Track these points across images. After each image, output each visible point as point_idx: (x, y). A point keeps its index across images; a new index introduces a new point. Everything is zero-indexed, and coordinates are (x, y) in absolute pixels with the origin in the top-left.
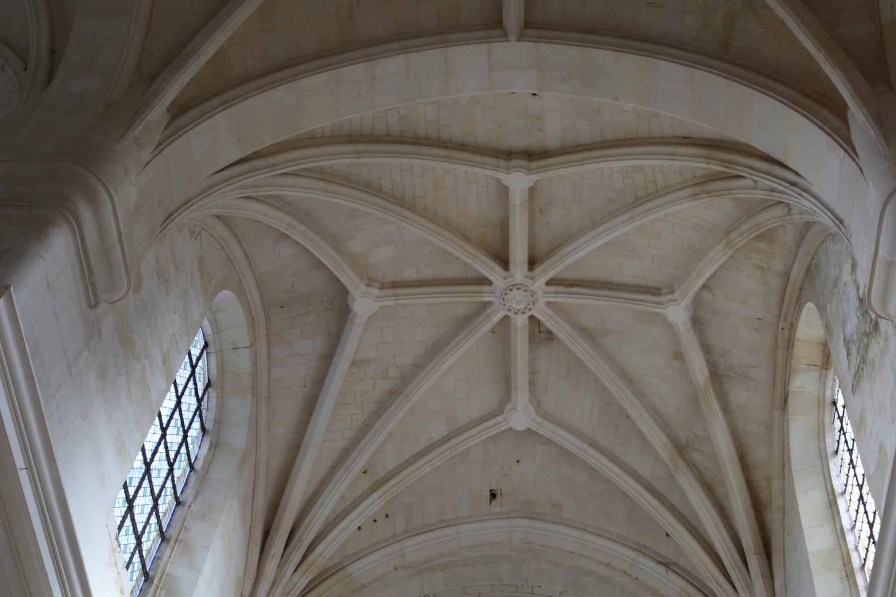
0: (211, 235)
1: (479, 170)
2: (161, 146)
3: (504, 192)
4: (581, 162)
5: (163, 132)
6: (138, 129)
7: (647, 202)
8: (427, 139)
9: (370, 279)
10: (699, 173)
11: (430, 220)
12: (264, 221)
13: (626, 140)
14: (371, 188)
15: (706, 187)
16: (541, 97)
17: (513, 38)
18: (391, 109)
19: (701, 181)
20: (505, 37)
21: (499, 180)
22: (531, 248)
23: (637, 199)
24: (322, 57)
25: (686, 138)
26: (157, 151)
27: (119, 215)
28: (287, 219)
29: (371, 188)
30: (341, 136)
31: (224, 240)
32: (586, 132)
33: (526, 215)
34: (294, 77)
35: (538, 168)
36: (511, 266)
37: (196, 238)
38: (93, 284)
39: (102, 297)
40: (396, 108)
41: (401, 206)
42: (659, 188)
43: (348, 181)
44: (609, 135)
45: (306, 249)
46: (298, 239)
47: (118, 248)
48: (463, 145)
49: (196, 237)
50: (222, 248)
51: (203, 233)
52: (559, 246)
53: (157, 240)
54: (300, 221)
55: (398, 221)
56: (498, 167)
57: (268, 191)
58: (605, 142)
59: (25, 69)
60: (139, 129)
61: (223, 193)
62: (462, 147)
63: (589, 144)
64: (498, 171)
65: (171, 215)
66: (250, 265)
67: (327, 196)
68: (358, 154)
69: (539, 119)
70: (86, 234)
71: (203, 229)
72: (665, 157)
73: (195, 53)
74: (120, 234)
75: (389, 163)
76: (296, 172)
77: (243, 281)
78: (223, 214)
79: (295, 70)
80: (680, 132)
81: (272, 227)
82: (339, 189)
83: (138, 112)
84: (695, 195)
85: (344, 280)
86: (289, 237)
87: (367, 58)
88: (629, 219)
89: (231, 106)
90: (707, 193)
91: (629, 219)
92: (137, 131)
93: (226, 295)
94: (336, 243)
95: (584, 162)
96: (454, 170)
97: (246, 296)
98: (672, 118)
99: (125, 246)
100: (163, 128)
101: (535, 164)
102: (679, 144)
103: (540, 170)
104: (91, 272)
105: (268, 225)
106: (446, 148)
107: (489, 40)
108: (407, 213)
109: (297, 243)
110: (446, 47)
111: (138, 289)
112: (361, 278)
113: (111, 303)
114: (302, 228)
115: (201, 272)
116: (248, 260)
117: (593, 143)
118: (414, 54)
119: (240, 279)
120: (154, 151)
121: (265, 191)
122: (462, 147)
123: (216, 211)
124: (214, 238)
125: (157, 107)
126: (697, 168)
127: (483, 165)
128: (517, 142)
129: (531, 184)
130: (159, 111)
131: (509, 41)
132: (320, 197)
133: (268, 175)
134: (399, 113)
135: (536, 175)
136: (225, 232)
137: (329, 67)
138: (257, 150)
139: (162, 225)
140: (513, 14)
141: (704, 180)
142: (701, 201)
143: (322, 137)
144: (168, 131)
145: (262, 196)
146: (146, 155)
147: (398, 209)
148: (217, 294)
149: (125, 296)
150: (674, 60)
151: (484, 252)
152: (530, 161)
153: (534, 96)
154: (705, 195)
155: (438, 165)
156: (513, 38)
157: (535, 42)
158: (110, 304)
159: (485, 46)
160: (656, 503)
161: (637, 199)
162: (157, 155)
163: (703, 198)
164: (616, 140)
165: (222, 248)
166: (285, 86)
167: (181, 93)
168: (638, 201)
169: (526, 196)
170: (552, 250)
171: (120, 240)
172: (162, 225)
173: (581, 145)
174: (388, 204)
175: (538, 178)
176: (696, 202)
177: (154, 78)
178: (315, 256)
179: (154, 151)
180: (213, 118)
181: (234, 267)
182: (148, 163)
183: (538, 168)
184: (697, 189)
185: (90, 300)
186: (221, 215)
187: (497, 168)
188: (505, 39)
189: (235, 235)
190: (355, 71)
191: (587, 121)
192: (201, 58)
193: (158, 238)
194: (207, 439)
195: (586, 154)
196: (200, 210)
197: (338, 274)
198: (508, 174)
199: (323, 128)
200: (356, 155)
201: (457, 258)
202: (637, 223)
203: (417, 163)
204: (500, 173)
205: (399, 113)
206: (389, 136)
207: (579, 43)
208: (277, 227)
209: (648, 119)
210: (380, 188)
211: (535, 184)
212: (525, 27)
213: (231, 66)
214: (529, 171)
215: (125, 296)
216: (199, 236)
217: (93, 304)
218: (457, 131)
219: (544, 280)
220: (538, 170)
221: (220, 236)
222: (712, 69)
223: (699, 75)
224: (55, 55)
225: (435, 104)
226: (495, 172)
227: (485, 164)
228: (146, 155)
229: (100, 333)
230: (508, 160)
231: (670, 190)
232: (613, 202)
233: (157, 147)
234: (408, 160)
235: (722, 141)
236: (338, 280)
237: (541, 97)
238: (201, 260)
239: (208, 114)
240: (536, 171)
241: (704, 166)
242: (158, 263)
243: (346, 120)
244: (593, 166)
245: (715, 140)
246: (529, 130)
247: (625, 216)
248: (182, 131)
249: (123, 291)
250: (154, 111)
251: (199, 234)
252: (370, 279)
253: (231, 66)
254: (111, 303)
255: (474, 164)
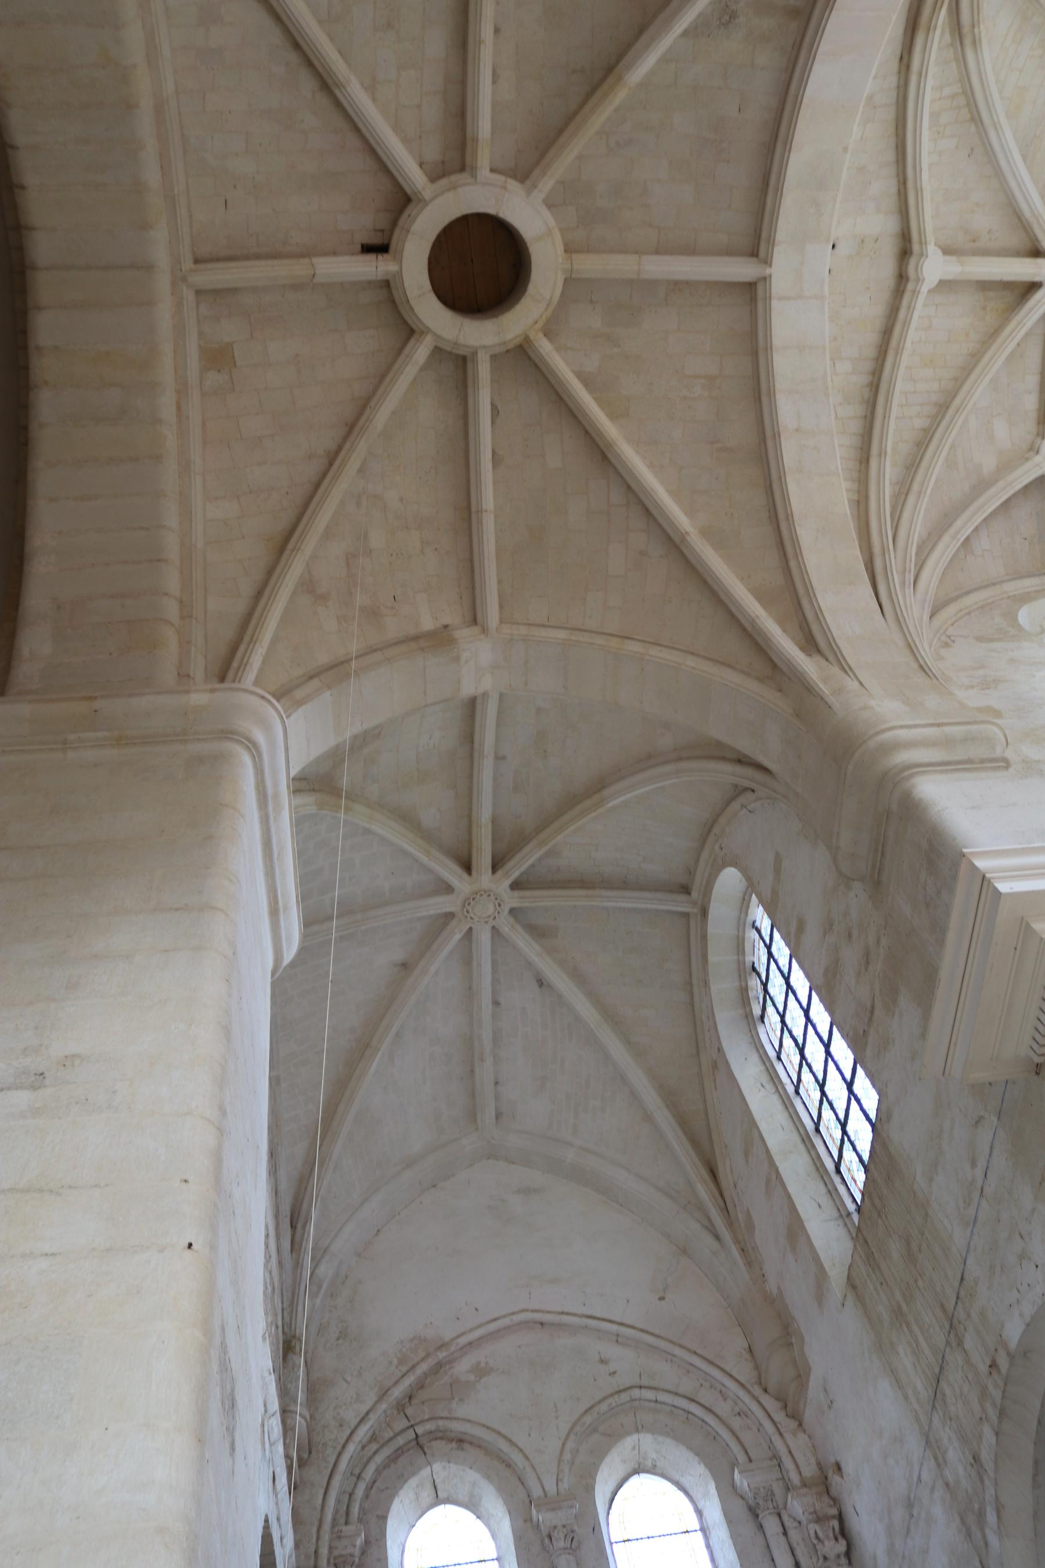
0: (952, 625)
1: (916, 314)
2: (846, 669)
3: (945, 286)
4: (919, 191)
5: (832, 664)
6: (824, 689)
7: (976, 106)
8: (874, 373)
9: (1030, 449)
10: (947, 38)
11: (968, 375)
12: (946, 564)
13: (897, 135)
14: (923, 442)
15: (966, 29)
16: (837, 239)
17: (768, 271)
18: (836, 413)
19: (957, 36)
20: (765, 279)
21: (929, 291)
22: (1019, 254)
23: (973, 119)
24: (771, 485)
25: (901, 58)
26: (850, 673)
27: (911, 723)
28: (946, 538)
29: (923, 442)
30: (860, 471)
31: (961, 610)
32: (884, 184)
33: (977, 259)
34: (789, 517)
35: (921, 243)
36: (1037, 279)
37: (954, 642)
38: (982, 761)
39: (998, 752)
40: (834, 407)
41: (947, 408)
42: (961, 90)
43: (912, 466)
44: (890, 156)
45: (985, 520)
46: (971, 529)
47: (947, 729)
48: (885, 333)
49: (952, 640)
50: (969, 613)
51: (948, 633)
52: (1019, 218)
53: (946, 686)
54: (950, 525)
55: (965, 412)
56: (914, 291)
57: (911, 556)
58: (897, 161)
59: (753, 791)
60: (824, 688)
61: (906, 606)
62: (887, 332)
63: (899, 181)
64: (919, 292)
65: (921, 667)
66: (994, 584)
67: (925, 493)
68: (882, 453)
69: (863, 241)
70: (927, 760)
71: (945, 632)
72: (922, 86)
73: (753, 620)
74: (931, 725)
75: (897, 418)
76: (895, 525)
77: (1012, 594)
78: (930, 609)
79: (781, 516)
80: (894, 65)
81: (954, 555)
82: (919, 478)
83: (808, 688)
84: (975, 43)
85: (1026, 481)
86: (968, 539)
87: (776, 436)
88: (996, 129)
89: (812, 588)
90: (973, 27)
91: (996, 129)
92: (827, 692)
93: (1024, 616)
94: (981, 486)
95: (919, 188)
96: (912, 343)
97: (1028, 593)
98: (875, 77)
99: (946, 721)
100: (827, 663)
101: (916, 247)
102: (908, 67)
103: (923, 241)
104: (969, 761)
105: (951, 561)
106: (886, 351)
107: (768, 298)
108: (957, 401)
109: (976, 529)
110: (771, 347)
111: (998, 714)
112: (1027, 459)
113: (1007, 744)
114: (959, 523)
115: (992, 640)
116: (988, 586)
117: (898, 176)
118: (777, 384)
119: (1009, 597)
120: (849, 676)
121: (911, 561)
122: (887, 332)
123: (926, 617)
124: (956, 621)
125: (805, 667)
126: (940, 42)
127: (911, 308)
128: (887, 269)
129: (940, 252)
130: (808, 666)
131: (770, 276)
132: (926, 500)
133: (892, 556)
134: (840, 404)
135: (928, 246)
136: (951, 610)
137: (783, 479)
138: (863, 566)
139: (930, 678)
140: (742, 270)
141: (957, 32)
142: (983, 35)
143: (859, 492)
144: (831, 658)
145: (916, 564)
146: (852, 684)
147: (951, 412)
148: (1020, 625)
149: (1002, 729)
150: (805, 78)
151: (1014, 313)
152: (911, 253)
153: (836, 247)
154: (976, 30)
155: (905, 360)
156: (768, 271)
157: (773, 245)
158: (1009, 746)
159: (775, 303)
160: (932, 52)
161: (973, 119)
162: (854, 674)
163: (980, 33)
164: (897, 147)
165: (969, 613)
166: (797, 528)
167: (793, 639)
168: (976, 118)
169: (954, 258)
170: (1024, 228)
171: (939, 725)
172: (930, 678)
173: (899, 190)
174: (944, 423)
175: (933, 243)
176: (984, 42)
177: (775, 666)
178: (994, 510)
179: (849, 676)
180: (823, 609)
181: (993, 602)
182: (861, 683)
183: (921, 243)
184: (968, 41)
185: (999, 767)
186: (931, 612)
187: (915, 293)
188: (768, 279)
189: (954, 599)
190: (790, 451)
191: (870, 183)
192: (759, 615)
193: (945, 684)
194: (749, 965)
195: (910, 184)
196: (921, 637)
197: (1019, 486)
198: (924, 280)
199: (848, 490)
200: (883, 456)
201: (1018, 345)
202: (1003, 119)
203: (900, 386)
204: (922, 290)
205: (840, 404)
206: (866, 416)
207: (779, 193)
208: (954, 550)
209: (875, 107)
210: (925, 430)
211: (940, 247)
212: (757, 256)
213: (771, 583)
214: (922, 255)
215: (1002, 729)
216: (951, 638)
217: (1005, 764)
218: (868, 338)
219: (508, 882)
220: (922, 243)
221: (955, 615)
222: (819, 30)
223: (825, 46)
224: (742, 760)
225: (834, 363)
226: (920, 296)
227: (909, 308)
228: (851, 684)
229: (1039, 761)
230: (908, 279)
231: (965, 77)
232: (972, 149)
233: (846, 672)
234: (895, 396)
235: (909, 11)
236: (1026, 487)
237: (837, 239)
238: (980, 639)
239: (818, 613)
240: (924, 246)
241: (938, 32)
242: (972, 687)
243: (841, 464)
244: (925, 175)
245: (907, 20)
246: (875, 253)
247: (992, 134)
248: (833, 643)
249: (996, 730)
250: (808, 671)
251: (949, 637)
252: (1030, 449)
253: (771, 583)
254: (1007, 744)
255: (907, 323)
